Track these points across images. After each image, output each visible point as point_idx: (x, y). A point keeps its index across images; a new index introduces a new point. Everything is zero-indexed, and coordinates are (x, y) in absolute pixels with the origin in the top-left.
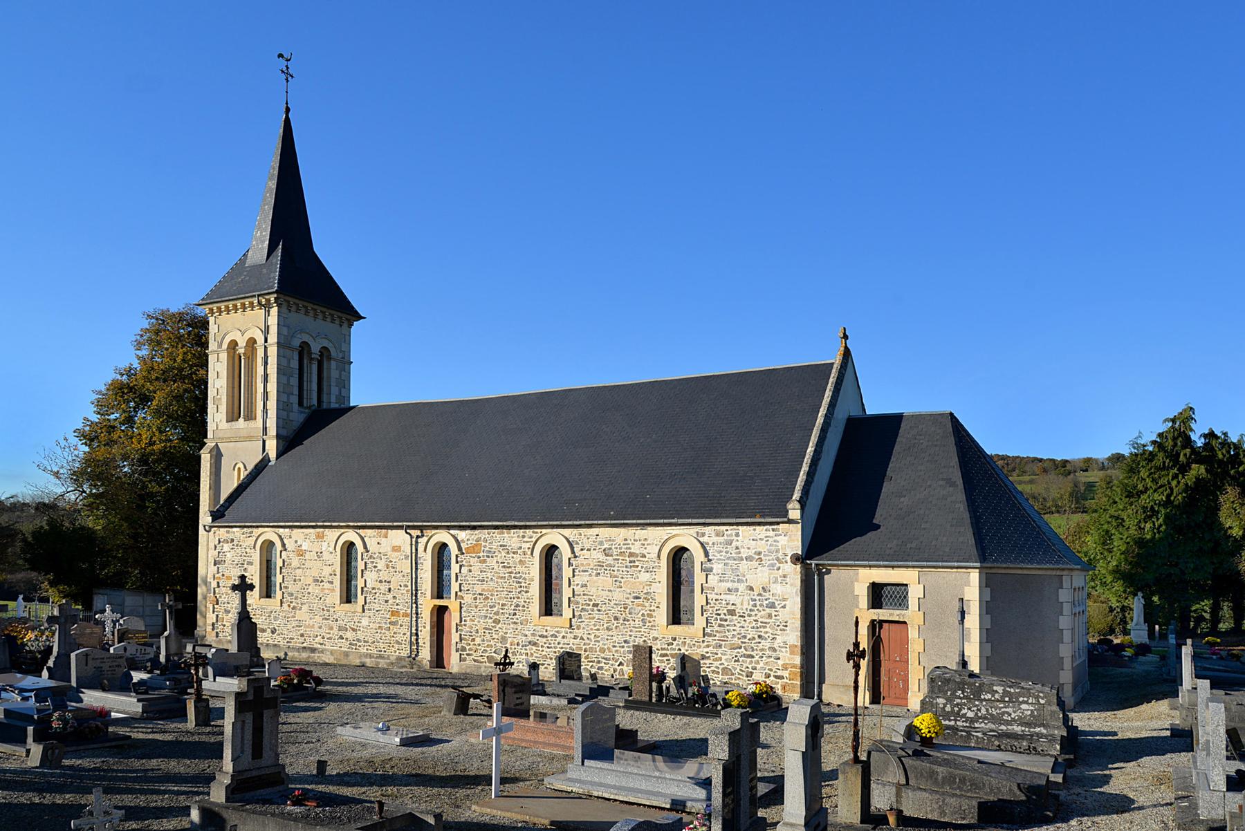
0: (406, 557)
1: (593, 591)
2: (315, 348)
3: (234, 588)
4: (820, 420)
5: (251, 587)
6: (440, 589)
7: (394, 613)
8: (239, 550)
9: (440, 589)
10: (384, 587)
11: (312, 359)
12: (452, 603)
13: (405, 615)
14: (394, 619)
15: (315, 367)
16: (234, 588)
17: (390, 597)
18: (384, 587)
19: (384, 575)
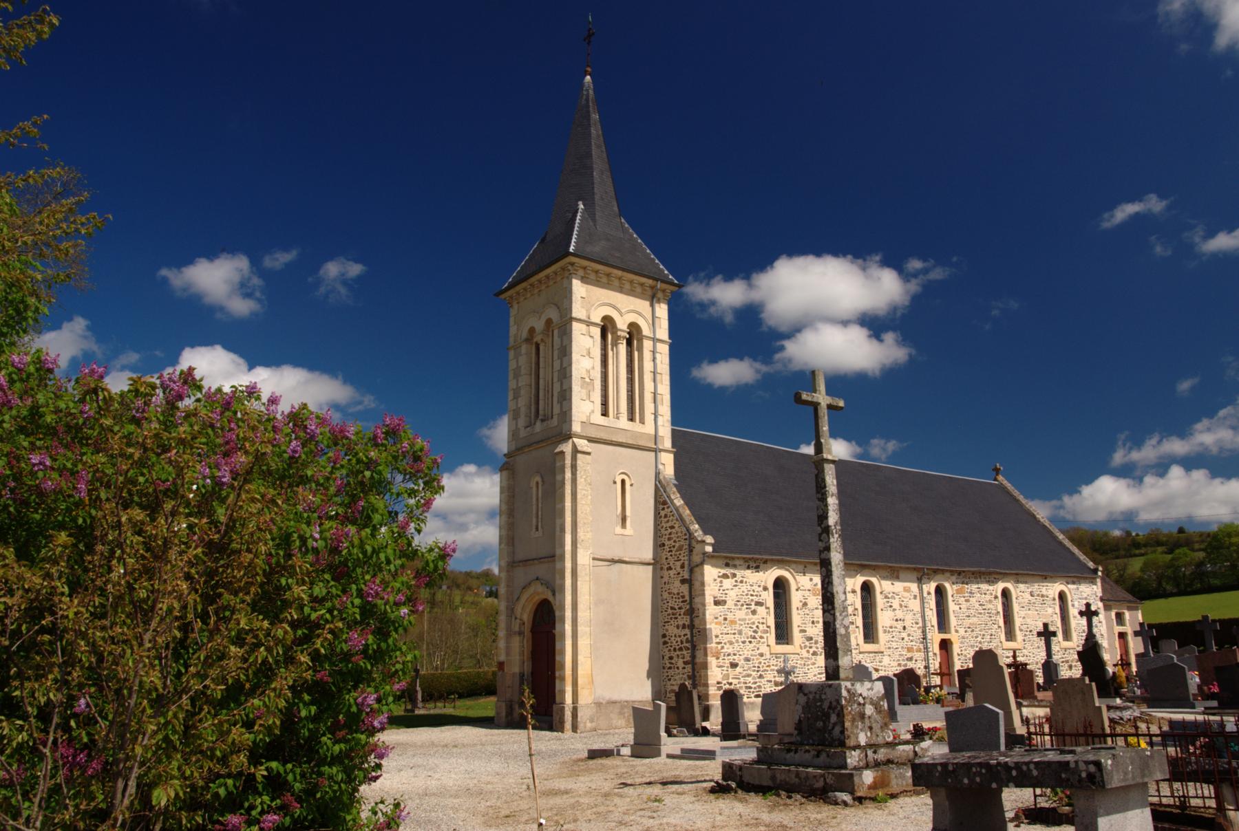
0: (915, 597)
1: (1028, 621)
2: (622, 324)
3: (1039, 634)
4: (832, 501)
5: (1054, 634)
6: (943, 624)
7: (910, 650)
8: (744, 588)
9: (943, 624)
10: (900, 625)
11: (619, 337)
12: (952, 636)
13: (919, 650)
14: (909, 655)
15: (623, 348)
16: (1039, 634)
17: (904, 635)
18: (900, 625)
19: (900, 614)
